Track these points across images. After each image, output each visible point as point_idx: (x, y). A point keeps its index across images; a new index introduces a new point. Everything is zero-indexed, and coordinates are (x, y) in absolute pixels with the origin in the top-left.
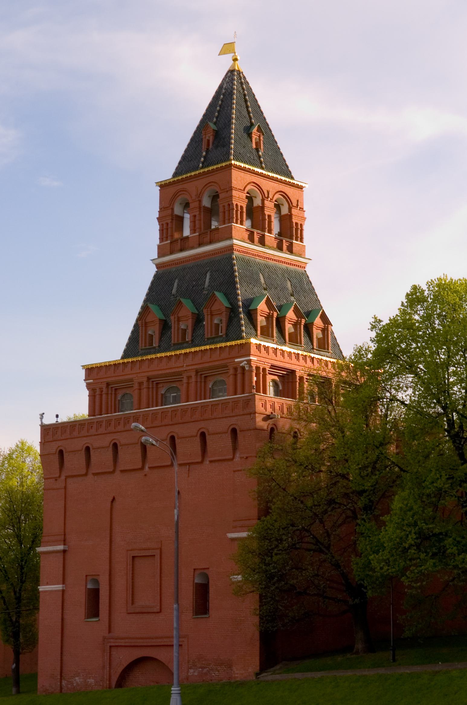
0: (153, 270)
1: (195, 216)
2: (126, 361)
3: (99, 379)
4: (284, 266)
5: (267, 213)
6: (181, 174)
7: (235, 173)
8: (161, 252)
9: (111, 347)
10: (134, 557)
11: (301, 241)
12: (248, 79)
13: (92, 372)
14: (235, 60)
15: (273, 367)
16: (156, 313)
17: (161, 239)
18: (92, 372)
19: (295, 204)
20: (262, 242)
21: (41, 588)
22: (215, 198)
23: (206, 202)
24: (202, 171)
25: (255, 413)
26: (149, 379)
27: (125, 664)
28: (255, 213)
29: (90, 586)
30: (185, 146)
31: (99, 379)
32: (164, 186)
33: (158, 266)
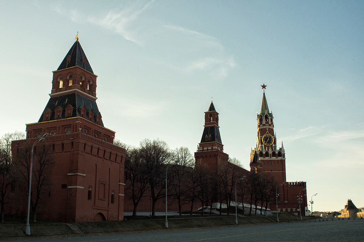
2: (40, 123)
3: (30, 128)
6: (60, 70)
8: (52, 92)
16: (50, 110)
17: (53, 89)
24: (67, 69)
25: (78, 154)
30: (40, 117)
31: (30, 128)
32: (54, 73)
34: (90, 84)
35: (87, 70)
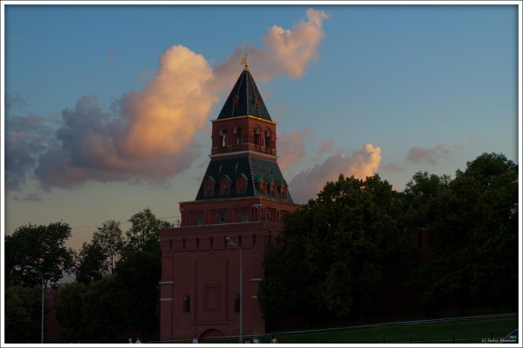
0: (210, 160)
1: (230, 138)
4: (268, 160)
5: (262, 137)
7: (250, 120)
8: (213, 152)
9: (191, 195)
10: (207, 287)
11: (275, 148)
12: (253, 78)
13: (183, 206)
14: (246, 66)
15: (268, 208)
17: (213, 146)
18: (183, 206)
19: (272, 132)
20: (260, 151)
21: (161, 300)
22: (239, 130)
23: (235, 132)
26: (212, 210)
27: (202, 332)
28: (257, 138)
29: (236, 298)
32: (214, 123)
33: (212, 158)
34: (257, 133)
35: (263, 118)
